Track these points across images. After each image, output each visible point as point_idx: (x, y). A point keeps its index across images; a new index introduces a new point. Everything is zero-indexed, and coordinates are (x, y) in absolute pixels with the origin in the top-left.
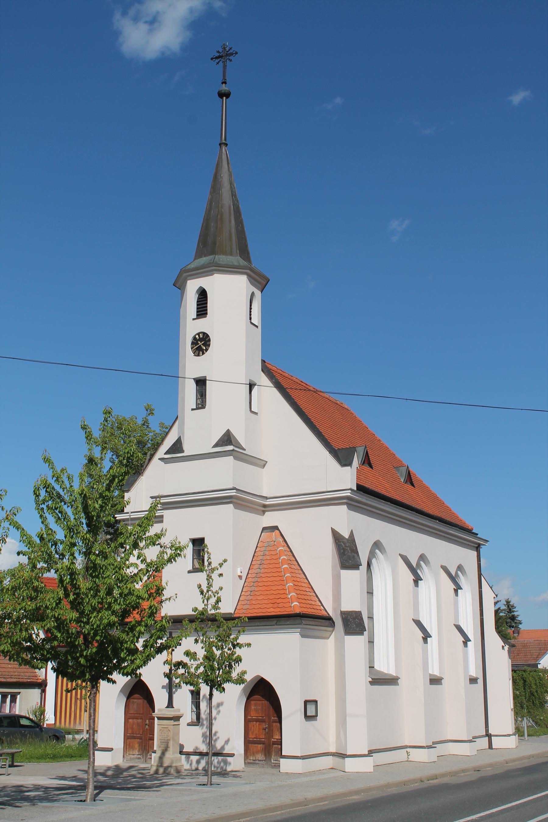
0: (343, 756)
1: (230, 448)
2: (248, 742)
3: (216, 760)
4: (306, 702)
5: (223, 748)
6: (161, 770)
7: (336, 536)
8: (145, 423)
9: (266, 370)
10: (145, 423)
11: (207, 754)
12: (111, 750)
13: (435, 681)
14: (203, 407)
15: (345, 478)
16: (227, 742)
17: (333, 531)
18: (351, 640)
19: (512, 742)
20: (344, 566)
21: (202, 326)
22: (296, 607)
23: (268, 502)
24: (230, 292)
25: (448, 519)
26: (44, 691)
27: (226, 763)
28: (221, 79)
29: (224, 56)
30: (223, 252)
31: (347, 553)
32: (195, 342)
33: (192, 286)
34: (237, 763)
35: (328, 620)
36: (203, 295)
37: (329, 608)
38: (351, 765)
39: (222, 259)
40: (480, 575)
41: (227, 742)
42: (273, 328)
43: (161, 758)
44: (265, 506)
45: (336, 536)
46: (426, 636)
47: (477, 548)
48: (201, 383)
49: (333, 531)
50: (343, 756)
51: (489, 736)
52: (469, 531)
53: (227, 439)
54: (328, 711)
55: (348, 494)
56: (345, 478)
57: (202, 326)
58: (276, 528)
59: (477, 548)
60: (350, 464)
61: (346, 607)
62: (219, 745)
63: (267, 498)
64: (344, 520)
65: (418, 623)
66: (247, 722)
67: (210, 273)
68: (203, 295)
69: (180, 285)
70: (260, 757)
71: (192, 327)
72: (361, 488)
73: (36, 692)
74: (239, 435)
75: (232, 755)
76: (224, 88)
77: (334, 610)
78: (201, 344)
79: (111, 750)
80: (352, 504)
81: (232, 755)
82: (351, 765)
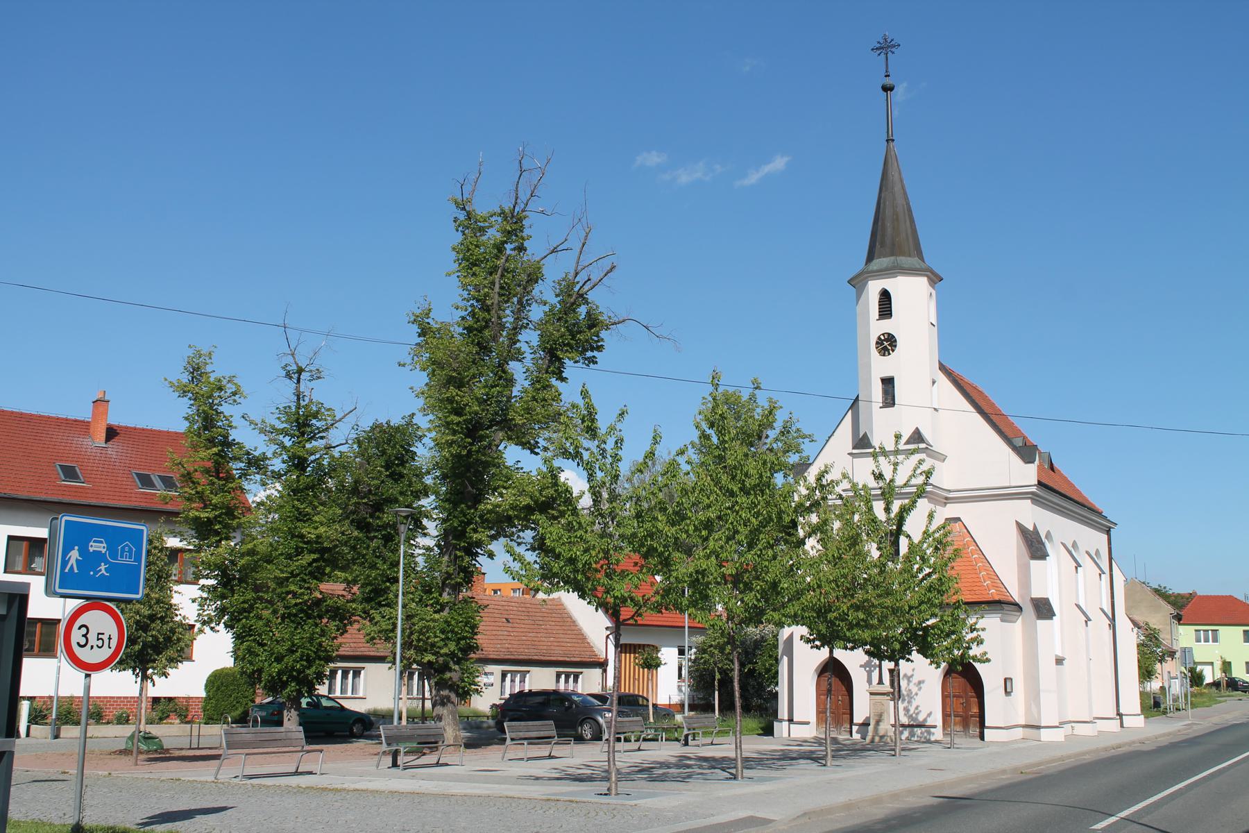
0: (1038, 727)
1: (922, 446)
2: (946, 716)
3: (918, 731)
4: (1005, 680)
5: (925, 720)
6: (877, 739)
7: (1022, 529)
8: (752, 398)
9: (942, 368)
10: (752, 398)
11: (909, 726)
12: (808, 723)
13: (1059, 661)
14: (893, 404)
15: (1028, 475)
16: (929, 715)
17: (1019, 525)
18: (1042, 624)
19: (1139, 722)
20: (1034, 557)
21: (886, 326)
22: (993, 594)
23: (951, 495)
24: (911, 292)
25: (1080, 500)
26: (605, 671)
27: (929, 733)
28: (884, 74)
29: (885, 47)
30: (902, 253)
31: (1034, 545)
32: (879, 342)
33: (874, 288)
34: (938, 734)
35: (1018, 607)
36: (885, 296)
37: (1015, 594)
38: (1046, 735)
39: (904, 260)
40: (1111, 559)
41: (929, 715)
42: (948, 327)
43: (876, 729)
44: (946, 498)
45: (1022, 529)
46: (1088, 619)
47: (1108, 532)
48: (888, 382)
49: (1019, 525)
50: (1038, 727)
51: (1120, 715)
52: (1099, 514)
53: (917, 437)
54: (1019, 686)
55: (1034, 489)
56: (1028, 475)
57: (886, 326)
58: (958, 519)
59: (1108, 532)
60: (1033, 462)
61: (1036, 594)
62: (921, 718)
63: (950, 491)
64: (1031, 515)
65: (1078, 606)
66: (944, 697)
67: (894, 275)
68: (885, 296)
69: (858, 282)
70: (958, 728)
71: (878, 328)
72: (1040, 483)
73: (598, 671)
74: (926, 434)
75: (935, 727)
76: (888, 81)
77: (1021, 596)
78: (887, 344)
79: (808, 723)
80: (1035, 499)
81: (935, 727)
82: (1046, 735)
